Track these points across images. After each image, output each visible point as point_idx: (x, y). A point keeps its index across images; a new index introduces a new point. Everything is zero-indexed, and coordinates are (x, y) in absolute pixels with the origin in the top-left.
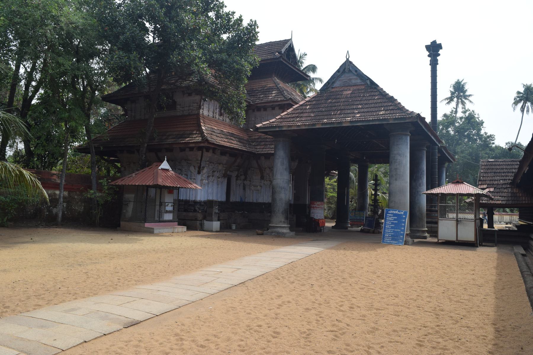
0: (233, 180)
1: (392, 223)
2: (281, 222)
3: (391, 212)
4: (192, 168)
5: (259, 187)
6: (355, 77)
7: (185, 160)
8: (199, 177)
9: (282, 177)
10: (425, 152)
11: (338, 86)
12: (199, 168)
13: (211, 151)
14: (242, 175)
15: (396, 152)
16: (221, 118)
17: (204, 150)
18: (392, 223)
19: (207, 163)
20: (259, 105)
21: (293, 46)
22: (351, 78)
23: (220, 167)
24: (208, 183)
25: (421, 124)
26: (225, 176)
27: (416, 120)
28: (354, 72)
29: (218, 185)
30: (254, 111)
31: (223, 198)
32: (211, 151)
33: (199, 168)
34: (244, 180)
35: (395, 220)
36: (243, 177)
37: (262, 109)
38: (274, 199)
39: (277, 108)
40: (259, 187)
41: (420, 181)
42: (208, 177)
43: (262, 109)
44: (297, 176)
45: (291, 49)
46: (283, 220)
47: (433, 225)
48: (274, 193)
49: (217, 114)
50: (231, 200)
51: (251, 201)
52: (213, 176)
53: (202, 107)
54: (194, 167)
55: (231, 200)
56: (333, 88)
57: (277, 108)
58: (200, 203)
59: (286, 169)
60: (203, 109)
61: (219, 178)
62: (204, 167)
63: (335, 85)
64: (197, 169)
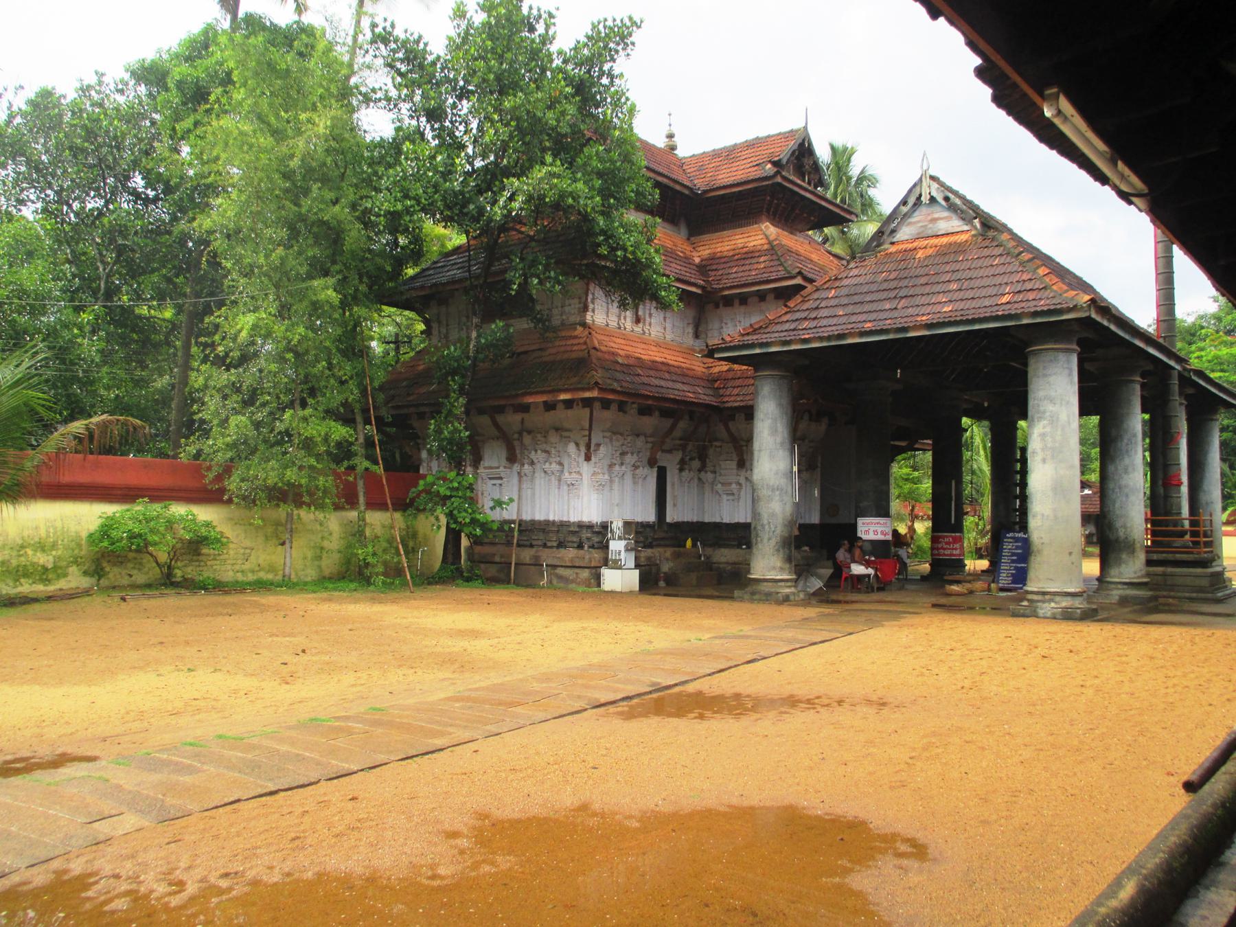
0: (672, 477)
1: (1013, 554)
2: (774, 568)
3: (1011, 535)
4: (572, 448)
5: (734, 486)
6: (946, 214)
7: (557, 430)
8: (586, 469)
9: (773, 460)
10: (1138, 387)
11: (906, 237)
12: (588, 446)
13: (614, 407)
14: (691, 459)
15: (1041, 394)
16: (638, 329)
17: (597, 405)
18: (1013, 554)
19: (608, 434)
20: (727, 293)
21: (810, 144)
22: (936, 216)
23: (640, 442)
24: (611, 481)
25: (1105, 323)
26: (652, 463)
27: (1086, 314)
28: (943, 203)
29: (635, 483)
30: (717, 306)
31: (650, 516)
32: (614, 407)
33: (588, 446)
34: (700, 471)
35: (1017, 548)
36: (696, 464)
37: (737, 302)
38: (756, 514)
39: (770, 297)
40: (734, 486)
41: (1127, 461)
42: (611, 466)
43: (737, 302)
44: (814, 459)
45: (803, 151)
46: (779, 564)
47: (1170, 570)
48: (755, 501)
49: (628, 320)
50: (668, 520)
51: (718, 520)
52: (622, 464)
53: (591, 306)
54: (577, 445)
55: (668, 520)
56: (893, 243)
57: (770, 297)
58: (590, 527)
59: (782, 444)
60: (593, 311)
61: (635, 467)
62: (598, 445)
63: (899, 236)
64: (583, 449)
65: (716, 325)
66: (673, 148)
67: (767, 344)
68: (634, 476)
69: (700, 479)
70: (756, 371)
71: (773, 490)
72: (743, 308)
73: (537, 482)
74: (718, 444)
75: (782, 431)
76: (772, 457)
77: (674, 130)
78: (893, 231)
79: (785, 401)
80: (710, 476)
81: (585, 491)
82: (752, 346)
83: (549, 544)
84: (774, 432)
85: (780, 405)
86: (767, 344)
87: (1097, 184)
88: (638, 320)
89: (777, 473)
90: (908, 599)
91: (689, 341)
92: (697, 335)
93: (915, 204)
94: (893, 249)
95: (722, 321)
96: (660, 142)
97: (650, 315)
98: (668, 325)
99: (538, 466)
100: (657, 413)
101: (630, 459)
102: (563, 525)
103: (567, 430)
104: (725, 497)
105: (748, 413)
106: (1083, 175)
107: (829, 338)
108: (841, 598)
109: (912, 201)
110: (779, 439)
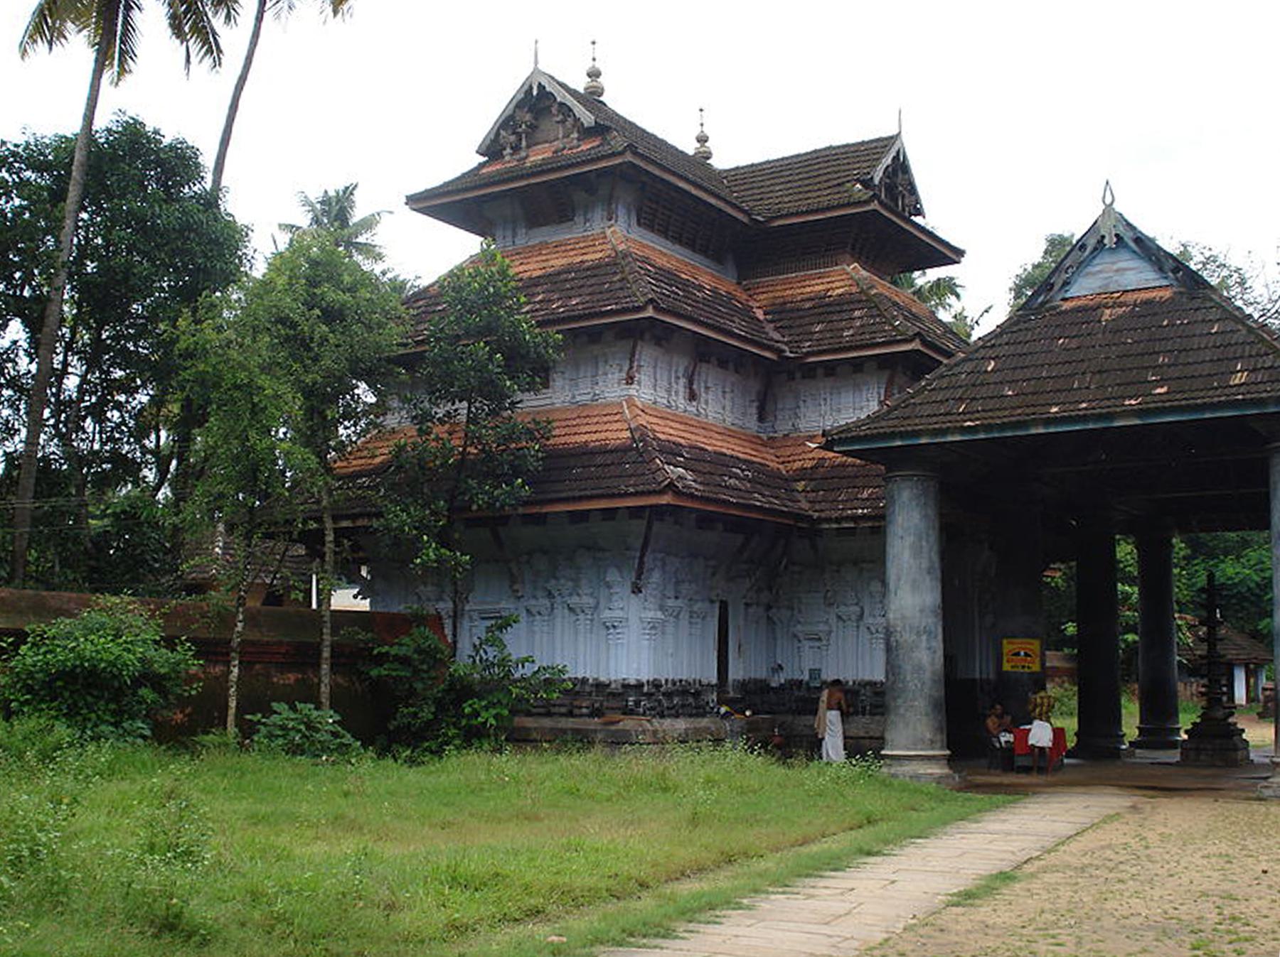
9: (911, 589)
28: (1132, 245)
37: (820, 371)
43: (820, 371)
63: (1073, 291)
68: (746, 614)
69: (769, 618)
70: (889, 470)
71: (918, 634)
72: (829, 382)
74: (796, 568)
75: (930, 555)
76: (915, 586)
77: (707, 131)
78: (1066, 283)
80: (785, 613)
81: (627, 639)
82: (893, 436)
83: (576, 711)
84: (917, 552)
87: (169, 31)
88: (692, 397)
89: (921, 611)
90: (1231, 784)
91: (752, 424)
92: (761, 419)
93: (1095, 249)
94: (1066, 306)
95: (797, 398)
97: (707, 388)
98: (728, 404)
100: (720, 526)
101: (684, 588)
102: (600, 686)
103: (603, 550)
104: (807, 644)
107: (1003, 427)
108: (1226, 786)
109: (1092, 242)
110: (925, 564)
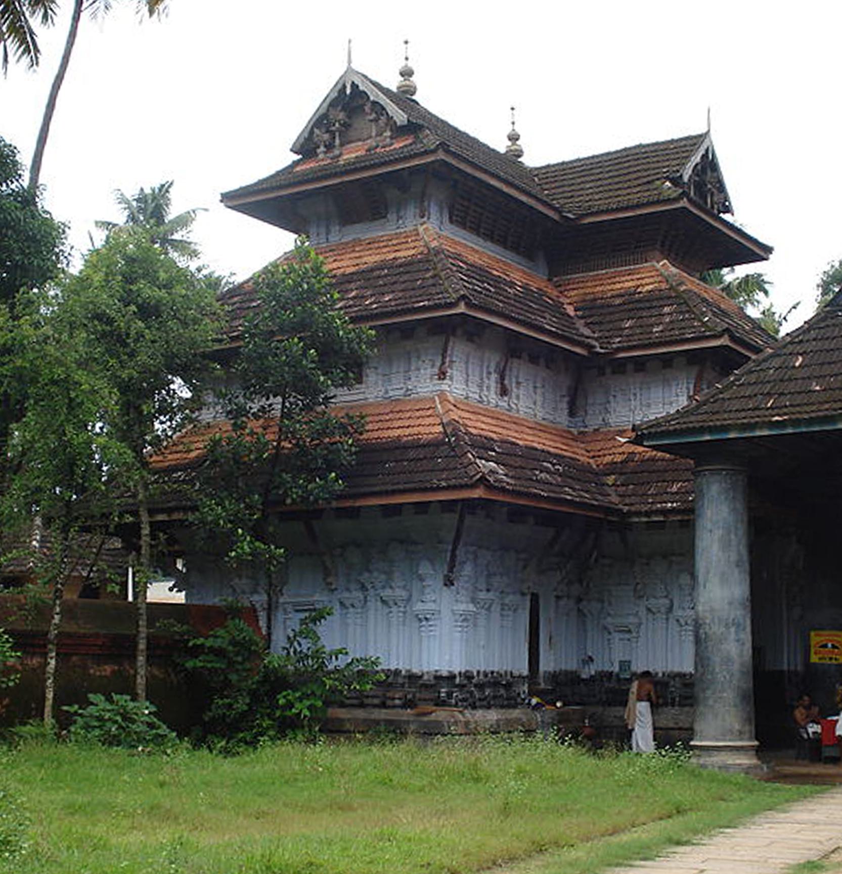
34: (33, 302)
37: (630, 367)
43: (630, 367)
65: (600, 398)
66: (520, 154)
67: (725, 429)
73: (371, 613)
75: (739, 548)
76: (724, 579)
79: (740, 506)
80: (596, 606)
81: (439, 630)
83: (389, 702)
84: (725, 545)
85: (734, 510)
86: (725, 429)
89: (730, 604)
91: (563, 418)
92: (572, 414)
95: (607, 393)
96: (501, 145)
97: (518, 383)
98: (539, 399)
99: (372, 592)
100: (531, 520)
101: (496, 581)
102: (413, 678)
104: (617, 636)
105: (686, 520)
106: (370, 77)
107: (810, 422)
110: (734, 557)
